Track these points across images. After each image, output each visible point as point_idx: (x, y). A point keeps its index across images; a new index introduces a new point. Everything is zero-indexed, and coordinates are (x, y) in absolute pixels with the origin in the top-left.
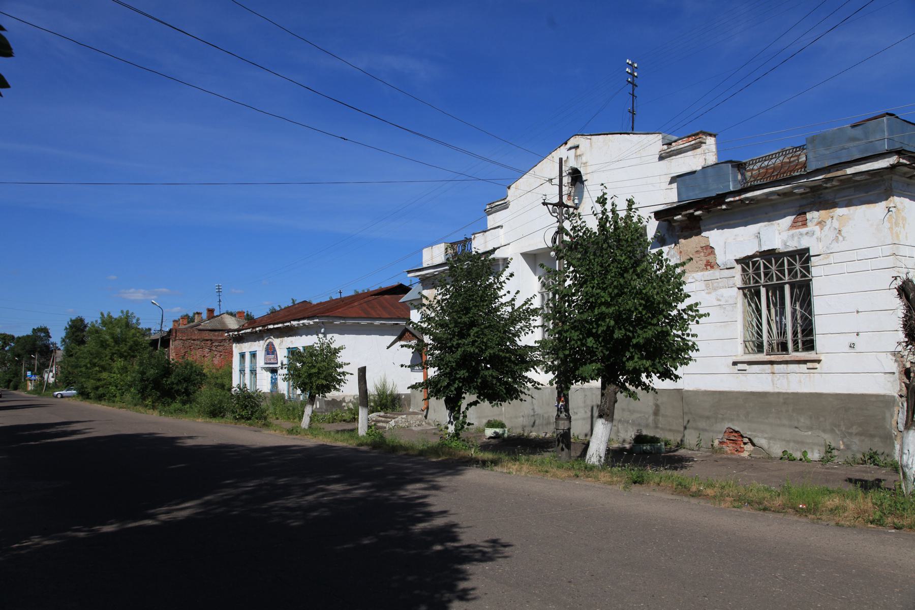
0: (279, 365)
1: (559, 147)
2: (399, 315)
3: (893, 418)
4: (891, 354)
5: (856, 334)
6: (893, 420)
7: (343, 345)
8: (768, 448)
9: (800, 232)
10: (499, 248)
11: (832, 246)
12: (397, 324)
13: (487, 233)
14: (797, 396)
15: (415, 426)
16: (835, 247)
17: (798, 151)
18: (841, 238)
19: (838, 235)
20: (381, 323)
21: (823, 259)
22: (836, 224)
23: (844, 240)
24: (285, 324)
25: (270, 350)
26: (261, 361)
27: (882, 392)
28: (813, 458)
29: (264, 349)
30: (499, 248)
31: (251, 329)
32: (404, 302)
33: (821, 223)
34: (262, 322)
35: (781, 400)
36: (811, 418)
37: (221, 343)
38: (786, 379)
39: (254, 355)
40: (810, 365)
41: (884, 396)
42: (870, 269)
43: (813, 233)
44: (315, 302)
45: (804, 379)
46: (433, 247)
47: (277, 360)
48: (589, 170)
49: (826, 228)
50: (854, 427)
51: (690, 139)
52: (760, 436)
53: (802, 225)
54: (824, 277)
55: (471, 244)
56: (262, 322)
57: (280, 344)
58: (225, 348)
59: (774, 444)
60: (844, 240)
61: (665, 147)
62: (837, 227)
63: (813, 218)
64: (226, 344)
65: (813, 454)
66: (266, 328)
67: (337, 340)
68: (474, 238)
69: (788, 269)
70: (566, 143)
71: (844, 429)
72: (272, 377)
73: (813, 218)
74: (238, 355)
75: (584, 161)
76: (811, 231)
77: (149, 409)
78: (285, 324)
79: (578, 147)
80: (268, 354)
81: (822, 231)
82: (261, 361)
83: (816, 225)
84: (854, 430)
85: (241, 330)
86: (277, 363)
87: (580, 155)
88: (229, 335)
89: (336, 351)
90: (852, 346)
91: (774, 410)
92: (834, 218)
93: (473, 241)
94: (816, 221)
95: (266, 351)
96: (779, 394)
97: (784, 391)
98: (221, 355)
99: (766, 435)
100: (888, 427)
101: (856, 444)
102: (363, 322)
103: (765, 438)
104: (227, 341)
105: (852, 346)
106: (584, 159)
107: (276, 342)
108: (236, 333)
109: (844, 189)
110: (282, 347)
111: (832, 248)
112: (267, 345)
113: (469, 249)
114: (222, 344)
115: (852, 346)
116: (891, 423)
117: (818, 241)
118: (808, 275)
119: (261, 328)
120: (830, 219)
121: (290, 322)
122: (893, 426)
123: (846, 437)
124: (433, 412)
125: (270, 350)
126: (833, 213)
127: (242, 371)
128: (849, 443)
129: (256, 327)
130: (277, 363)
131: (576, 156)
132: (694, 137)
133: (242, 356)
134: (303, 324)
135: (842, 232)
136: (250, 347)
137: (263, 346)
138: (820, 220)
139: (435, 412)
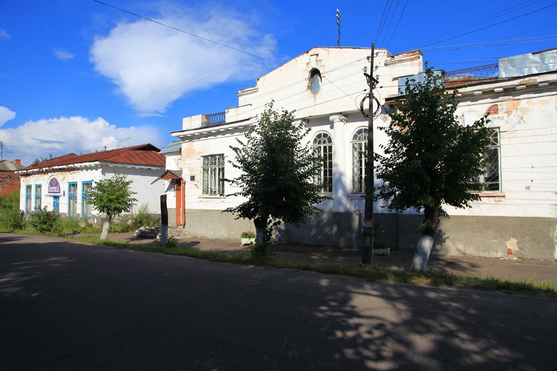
0: (62, 193)
1: (302, 55)
2: (151, 163)
3: (555, 231)
4: (555, 193)
5: (531, 180)
6: (555, 232)
7: (131, 180)
8: (464, 250)
9: (493, 117)
10: (252, 118)
11: (515, 126)
12: (150, 169)
13: (238, 108)
14: (486, 218)
15: (176, 236)
16: (518, 127)
17: (487, 68)
18: (522, 122)
19: (520, 120)
20: (140, 168)
21: (509, 134)
22: (519, 113)
23: (524, 123)
24: (69, 166)
25: (54, 183)
26: (45, 190)
27: (548, 216)
28: (497, 256)
29: (49, 183)
30: (252, 118)
31: (38, 169)
32: (162, 154)
33: (508, 113)
34: (43, 165)
35: (475, 221)
36: (496, 231)
37: (4, 179)
38: (479, 208)
39: (39, 187)
40: (497, 199)
41: (549, 218)
42: (542, 141)
43: (503, 118)
44: (470, 102)
45: (492, 208)
46: (192, 117)
47: (60, 190)
48: (327, 69)
49: (512, 115)
50: (527, 237)
51: (409, 55)
52: (458, 243)
53: (494, 113)
54: (509, 145)
55: (225, 116)
56: (43, 165)
57: (62, 179)
58: (7, 183)
59: (469, 248)
60: (524, 123)
61: (389, 58)
62: (520, 115)
63: (503, 109)
64: (7, 180)
65: (497, 254)
66: (52, 168)
67: (128, 178)
68: (228, 112)
69: (327, 152)
70: (308, 52)
71: (519, 238)
72: (54, 202)
73: (503, 109)
74: (25, 188)
75: (323, 65)
76: (501, 117)
77: (423, 279)
78: (69, 166)
79: (317, 55)
80: (52, 186)
81: (509, 117)
82: (45, 190)
83: (505, 113)
84: (527, 239)
85: (29, 170)
86: (59, 192)
87: (320, 61)
88: (19, 173)
89: (128, 183)
90: (528, 188)
91: (468, 226)
92: (518, 109)
93: (226, 114)
94: (504, 111)
95: (49, 184)
96: (473, 217)
97: (477, 215)
98: (4, 187)
99: (462, 243)
100: (551, 237)
101: (528, 247)
102: (129, 166)
103: (462, 244)
104: (8, 178)
105: (528, 188)
106: (323, 63)
107: (59, 176)
108: (25, 171)
109: (209, 134)
110: (65, 181)
111: (516, 128)
112: (51, 180)
113: (223, 119)
114: (4, 180)
115: (528, 188)
116: (553, 235)
117: (506, 123)
118: (496, 144)
119: (47, 168)
120: (515, 110)
121: (73, 164)
122: (554, 236)
123: (521, 243)
124: (189, 226)
125: (54, 183)
126: (517, 107)
127: (28, 198)
128: (523, 246)
129: (43, 168)
130: (59, 192)
131: (317, 61)
132: (412, 54)
133: (29, 187)
134: (85, 166)
135: (523, 118)
136: (36, 181)
137: (48, 181)
138: (508, 110)
139: (190, 226)
